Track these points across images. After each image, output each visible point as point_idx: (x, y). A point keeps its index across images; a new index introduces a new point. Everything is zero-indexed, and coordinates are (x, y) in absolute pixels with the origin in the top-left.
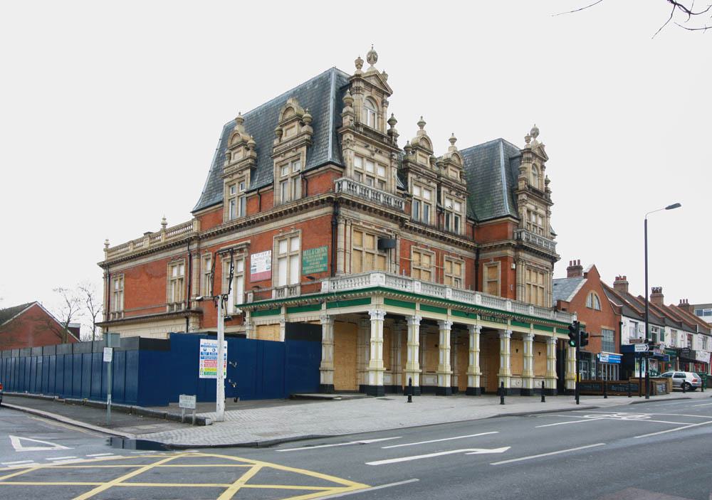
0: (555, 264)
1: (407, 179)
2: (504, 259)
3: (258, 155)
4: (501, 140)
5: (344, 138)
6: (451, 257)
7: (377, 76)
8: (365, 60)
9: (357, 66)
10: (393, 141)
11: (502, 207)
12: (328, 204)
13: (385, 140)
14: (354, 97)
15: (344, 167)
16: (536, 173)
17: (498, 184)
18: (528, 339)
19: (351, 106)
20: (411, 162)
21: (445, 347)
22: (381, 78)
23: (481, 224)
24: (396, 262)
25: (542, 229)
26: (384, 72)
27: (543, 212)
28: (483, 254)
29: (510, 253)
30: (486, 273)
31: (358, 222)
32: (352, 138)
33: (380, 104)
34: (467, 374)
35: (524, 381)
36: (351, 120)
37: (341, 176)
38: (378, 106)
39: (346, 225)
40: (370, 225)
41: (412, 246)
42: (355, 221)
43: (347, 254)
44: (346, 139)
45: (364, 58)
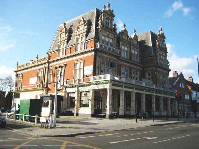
2: (152, 70)
13: (113, 31)
27: (164, 55)
29: (154, 68)
33: (111, 20)
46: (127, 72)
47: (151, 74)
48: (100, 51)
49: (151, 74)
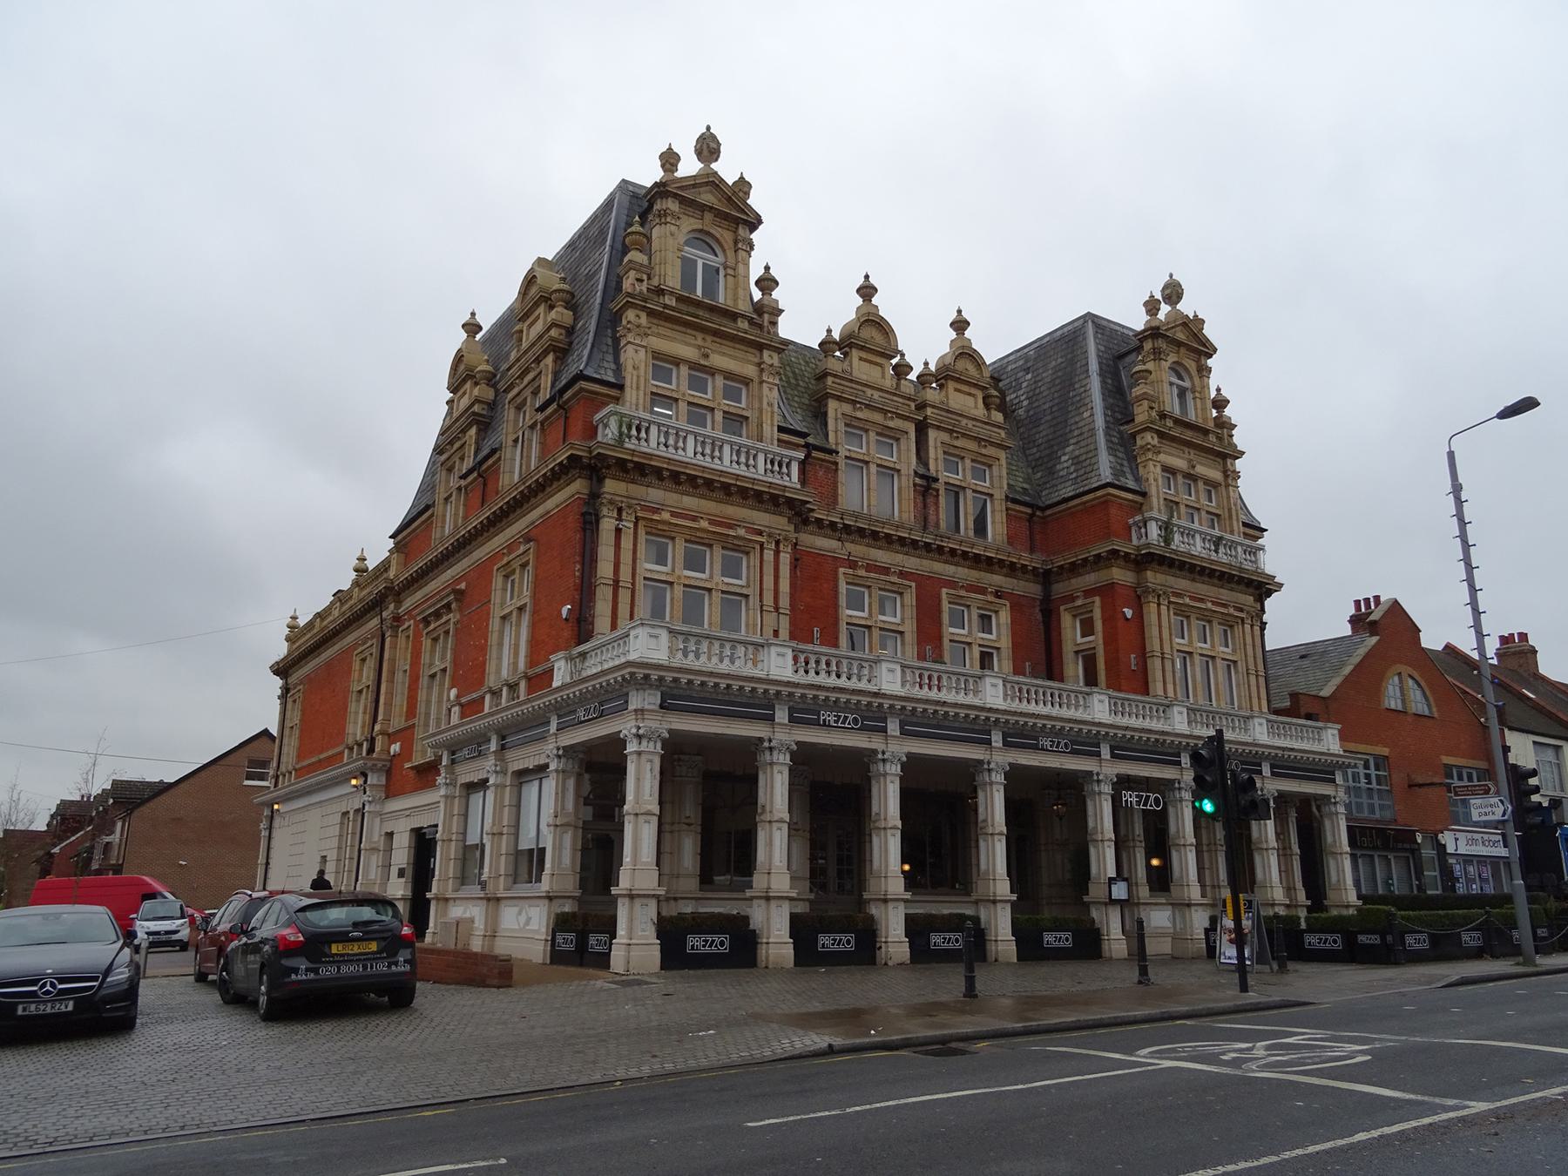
0: (1269, 603)
1: (825, 414)
2: (1107, 591)
3: (496, 396)
4: (1090, 317)
5: (1139, 442)
11: (1093, 467)
12: (575, 472)
13: (1212, 438)
15: (1144, 494)
16: (1187, 384)
17: (1086, 415)
20: (835, 376)
22: (1193, 326)
23: (1049, 512)
24: (777, 609)
25: (1218, 516)
27: (1215, 474)
28: (1061, 585)
29: (1121, 575)
30: (1071, 634)
31: (656, 511)
32: (1155, 441)
33: (1194, 372)
34: (1086, 899)
35: (1177, 912)
36: (1152, 408)
38: (1191, 378)
39: (1159, 605)
40: (694, 519)
41: (841, 570)
42: (645, 508)
43: (1260, 678)
45: (1158, 296)
46: (901, 614)
47: (1097, 614)
48: (622, 464)
49: (1097, 614)
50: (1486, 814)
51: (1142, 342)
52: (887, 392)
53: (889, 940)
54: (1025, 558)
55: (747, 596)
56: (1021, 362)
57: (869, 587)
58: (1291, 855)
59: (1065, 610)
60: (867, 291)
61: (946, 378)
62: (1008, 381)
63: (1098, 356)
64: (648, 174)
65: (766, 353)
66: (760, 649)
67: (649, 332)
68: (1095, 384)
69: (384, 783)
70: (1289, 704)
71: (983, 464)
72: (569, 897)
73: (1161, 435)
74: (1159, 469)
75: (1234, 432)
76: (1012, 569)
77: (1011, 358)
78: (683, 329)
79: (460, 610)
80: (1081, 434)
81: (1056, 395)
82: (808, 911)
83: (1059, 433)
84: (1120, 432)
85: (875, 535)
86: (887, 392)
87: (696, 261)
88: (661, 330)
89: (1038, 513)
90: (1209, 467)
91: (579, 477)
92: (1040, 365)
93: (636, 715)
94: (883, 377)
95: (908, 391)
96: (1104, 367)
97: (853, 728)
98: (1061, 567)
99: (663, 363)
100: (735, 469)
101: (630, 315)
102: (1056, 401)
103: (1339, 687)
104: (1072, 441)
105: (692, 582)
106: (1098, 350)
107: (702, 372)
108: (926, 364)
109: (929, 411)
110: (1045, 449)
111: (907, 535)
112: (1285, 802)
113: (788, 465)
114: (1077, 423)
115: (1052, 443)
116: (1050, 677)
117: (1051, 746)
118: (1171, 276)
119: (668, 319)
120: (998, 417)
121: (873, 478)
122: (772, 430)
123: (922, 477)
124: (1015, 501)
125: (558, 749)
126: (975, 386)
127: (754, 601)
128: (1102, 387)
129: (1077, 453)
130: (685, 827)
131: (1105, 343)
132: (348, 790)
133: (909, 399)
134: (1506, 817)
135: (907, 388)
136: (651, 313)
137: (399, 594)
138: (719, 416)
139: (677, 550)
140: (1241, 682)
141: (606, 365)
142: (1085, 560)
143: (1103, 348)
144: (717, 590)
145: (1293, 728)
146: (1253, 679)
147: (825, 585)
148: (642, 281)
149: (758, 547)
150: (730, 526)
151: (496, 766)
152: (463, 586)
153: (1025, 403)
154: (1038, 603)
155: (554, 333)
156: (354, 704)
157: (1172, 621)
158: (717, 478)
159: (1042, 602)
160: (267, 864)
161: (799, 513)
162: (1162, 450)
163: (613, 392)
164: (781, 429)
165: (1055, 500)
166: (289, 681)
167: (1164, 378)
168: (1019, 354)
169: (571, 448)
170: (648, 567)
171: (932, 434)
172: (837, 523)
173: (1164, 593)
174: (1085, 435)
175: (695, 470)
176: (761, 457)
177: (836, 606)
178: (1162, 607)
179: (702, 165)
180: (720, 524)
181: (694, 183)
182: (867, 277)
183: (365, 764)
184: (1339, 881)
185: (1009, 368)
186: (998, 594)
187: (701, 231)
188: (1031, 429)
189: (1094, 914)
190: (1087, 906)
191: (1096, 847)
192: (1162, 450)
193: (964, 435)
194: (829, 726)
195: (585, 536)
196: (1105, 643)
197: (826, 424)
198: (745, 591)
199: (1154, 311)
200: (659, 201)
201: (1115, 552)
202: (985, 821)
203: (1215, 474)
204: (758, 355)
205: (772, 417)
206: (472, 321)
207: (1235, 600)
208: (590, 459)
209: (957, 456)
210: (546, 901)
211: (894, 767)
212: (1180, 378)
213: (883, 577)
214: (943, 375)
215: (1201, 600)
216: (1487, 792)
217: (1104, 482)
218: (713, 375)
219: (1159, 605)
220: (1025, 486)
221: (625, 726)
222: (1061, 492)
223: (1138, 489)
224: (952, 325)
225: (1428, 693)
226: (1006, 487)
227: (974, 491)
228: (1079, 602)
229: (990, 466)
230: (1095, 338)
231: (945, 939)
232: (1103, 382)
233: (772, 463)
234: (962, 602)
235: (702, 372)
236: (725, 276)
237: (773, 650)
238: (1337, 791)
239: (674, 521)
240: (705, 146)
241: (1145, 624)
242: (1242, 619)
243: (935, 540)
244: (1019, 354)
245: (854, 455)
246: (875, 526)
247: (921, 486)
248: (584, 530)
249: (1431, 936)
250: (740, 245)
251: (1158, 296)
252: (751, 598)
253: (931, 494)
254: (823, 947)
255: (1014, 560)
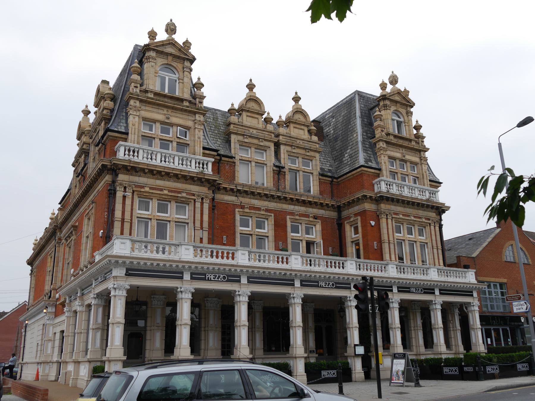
0: (444, 216)
1: (230, 141)
2: (363, 214)
5: (378, 146)
6: (297, 217)
7: (399, 93)
8: (387, 82)
9: (149, 37)
10: (420, 142)
11: (357, 158)
14: (383, 113)
15: (380, 170)
16: (402, 120)
17: (355, 135)
18: (473, 308)
19: (381, 120)
20: (234, 124)
21: (351, 326)
23: (339, 180)
24: (202, 228)
25: (418, 178)
26: (405, 89)
27: (416, 159)
28: (345, 212)
29: (368, 206)
30: (350, 234)
31: (143, 187)
32: (385, 145)
33: (405, 114)
34: (346, 354)
37: (379, 177)
38: (403, 117)
39: (387, 219)
42: (395, 214)
43: (439, 250)
44: (379, 147)
45: (387, 81)
47: (359, 225)
49: (359, 225)
50: (519, 309)
51: (379, 102)
52: (260, 130)
53: (298, 374)
54: (328, 201)
55: (188, 223)
56: (331, 114)
57: (251, 217)
58: (456, 330)
59: (347, 223)
60: (251, 86)
61: (289, 122)
62: (326, 123)
63: (361, 109)
64: (145, 40)
65: (197, 116)
66: (177, 246)
67: (140, 109)
68: (358, 122)
69: (54, 311)
70: (456, 262)
71: (308, 159)
72: (120, 360)
73: (388, 143)
74: (386, 158)
75: (424, 140)
76: (322, 206)
77: (327, 112)
78: (157, 107)
79: (76, 234)
80: (352, 144)
81: (344, 128)
82: (315, 361)
83: (344, 144)
84: (369, 142)
85: (253, 193)
86: (260, 130)
87: (165, 77)
88: (147, 108)
89: (335, 180)
90: (413, 156)
91: (108, 174)
92: (338, 114)
93: (114, 279)
94: (258, 123)
95: (270, 129)
96: (363, 114)
97: (223, 281)
98: (344, 204)
99: (149, 122)
100: (180, 167)
101: (132, 102)
102: (344, 130)
103: (480, 253)
104: (349, 147)
105: (160, 218)
106: (361, 106)
107: (166, 125)
108: (280, 117)
109: (281, 137)
110: (339, 151)
111: (268, 193)
112: (453, 306)
113: (207, 164)
114: (351, 139)
115: (342, 149)
116: (342, 256)
117: (325, 285)
118: (393, 72)
119: (150, 103)
120: (315, 138)
121: (253, 168)
122: (200, 149)
123: (276, 166)
124: (322, 175)
125: (94, 295)
126: (304, 125)
127: (191, 225)
128: (362, 123)
129: (351, 153)
130: (156, 328)
131: (364, 103)
132: (42, 315)
133: (271, 132)
134: (527, 310)
135: (270, 127)
136: (141, 101)
137: (61, 228)
138: (175, 144)
139: (154, 204)
140: (430, 252)
141: (121, 124)
142: (353, 200)
143: (363, 106)
144: (173, 221)
145: (452, 272)
146: (435, 250)
147: (229, 217)
148: (137, 87)
149: (428, 225)
150: (180, 193)
151: (79, 303)
152: (77, 224)
153: (332, 132)
154: (336, 220)
155: (105, 112)
156: (48, 277)
157: (394, 226)
158: (171, 172)
159: (337, 220)
160: (24, 347)
161: (214, 186)
162: (387, 149)
163: (124, 136)
164: (204, 148)
165: (342, 174)
166: (33, 267)
167: (389, 118)
168: (330, 110)
169: (102, 161)
170: (139, 212)
171: (282, 147)
172: (233, 189)
173: (390, 214)
174: (354, 145)
175: (160, 168)
176: (193, 162)
177: (234, 226)
178: (389, 220)
179: (168, 36)
180: (175, 192)
181: (163, 44)
182: (251, 80)
183: (45, 303)
184: (476, 341)
185: (326, 117)
186: (315, 217)
187: (167, 64)
188: (334, 143)
189: (349, 361)
190: (346, 357)
191: (392, 331)
192: (387, 149)
193: (298, 147)
194: (211, 280)
195: (109, 199)
196: (363, 237)
197: (230, 145)
198: (187, 221)
199: (384, 88)
200: (147, 53)
201: (365, 196)
202: (292, 321)
203: (416, 159)
204: (419, 154)
205: (200, 143)
206: (86, 109)
207: (426, 215)
208: (111, 166)
209: (295, 157)
210: (88, 363)
211: (244, 298)
212: (399, 117)
213: (257, 212)
214: (288, 122)
215: (409, 216)
216: (520, 299)
217: (360, 165)
218: (172, 126)
219: (387, 219)
220: (330, 168)
221: (109, 285)
222: (345, 170)
223: (377, 167)
224: (293, 99)
225: (527, 253)
226: (319, 170)
227: (303, 172)
228: (352, 219)
229: (312, 160)
230: (359, 101)
231: (450, 370)
232: (362, 121)
233: (199, 163)
234: (298, 222)
235: (166, 125)
236: (179, 83)
237: (183, 247)
238: (474, 302)
239: (151, 191)
240: (169, 28)
241: (381, 228)
242: (430, 224)
243: (282, 194)
244: (330, 110)
245: (244, 159)
246: (253, 189)
247: (276, 171)
248: (109, 197)
249: (500, 367)
250: (185, 69)
251: (387, 81)
252: (189, 224)
253: (282, 174)
254: (324, 376)
255: (322, 202)
